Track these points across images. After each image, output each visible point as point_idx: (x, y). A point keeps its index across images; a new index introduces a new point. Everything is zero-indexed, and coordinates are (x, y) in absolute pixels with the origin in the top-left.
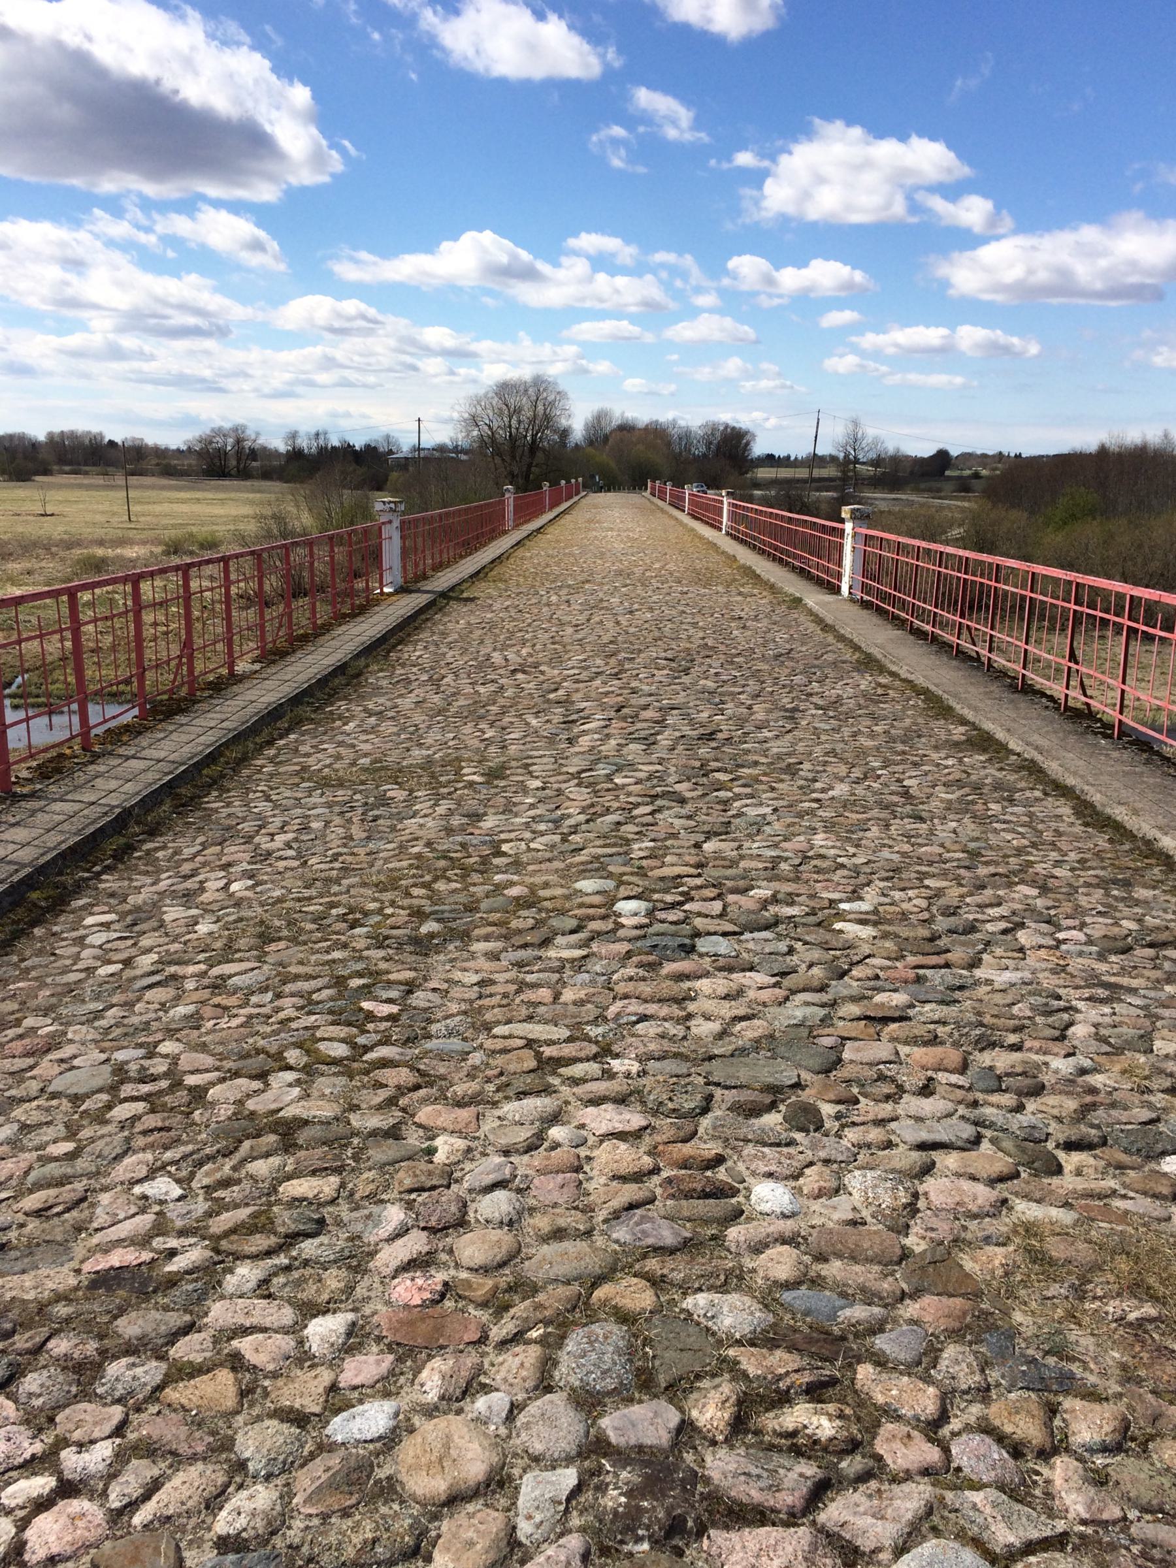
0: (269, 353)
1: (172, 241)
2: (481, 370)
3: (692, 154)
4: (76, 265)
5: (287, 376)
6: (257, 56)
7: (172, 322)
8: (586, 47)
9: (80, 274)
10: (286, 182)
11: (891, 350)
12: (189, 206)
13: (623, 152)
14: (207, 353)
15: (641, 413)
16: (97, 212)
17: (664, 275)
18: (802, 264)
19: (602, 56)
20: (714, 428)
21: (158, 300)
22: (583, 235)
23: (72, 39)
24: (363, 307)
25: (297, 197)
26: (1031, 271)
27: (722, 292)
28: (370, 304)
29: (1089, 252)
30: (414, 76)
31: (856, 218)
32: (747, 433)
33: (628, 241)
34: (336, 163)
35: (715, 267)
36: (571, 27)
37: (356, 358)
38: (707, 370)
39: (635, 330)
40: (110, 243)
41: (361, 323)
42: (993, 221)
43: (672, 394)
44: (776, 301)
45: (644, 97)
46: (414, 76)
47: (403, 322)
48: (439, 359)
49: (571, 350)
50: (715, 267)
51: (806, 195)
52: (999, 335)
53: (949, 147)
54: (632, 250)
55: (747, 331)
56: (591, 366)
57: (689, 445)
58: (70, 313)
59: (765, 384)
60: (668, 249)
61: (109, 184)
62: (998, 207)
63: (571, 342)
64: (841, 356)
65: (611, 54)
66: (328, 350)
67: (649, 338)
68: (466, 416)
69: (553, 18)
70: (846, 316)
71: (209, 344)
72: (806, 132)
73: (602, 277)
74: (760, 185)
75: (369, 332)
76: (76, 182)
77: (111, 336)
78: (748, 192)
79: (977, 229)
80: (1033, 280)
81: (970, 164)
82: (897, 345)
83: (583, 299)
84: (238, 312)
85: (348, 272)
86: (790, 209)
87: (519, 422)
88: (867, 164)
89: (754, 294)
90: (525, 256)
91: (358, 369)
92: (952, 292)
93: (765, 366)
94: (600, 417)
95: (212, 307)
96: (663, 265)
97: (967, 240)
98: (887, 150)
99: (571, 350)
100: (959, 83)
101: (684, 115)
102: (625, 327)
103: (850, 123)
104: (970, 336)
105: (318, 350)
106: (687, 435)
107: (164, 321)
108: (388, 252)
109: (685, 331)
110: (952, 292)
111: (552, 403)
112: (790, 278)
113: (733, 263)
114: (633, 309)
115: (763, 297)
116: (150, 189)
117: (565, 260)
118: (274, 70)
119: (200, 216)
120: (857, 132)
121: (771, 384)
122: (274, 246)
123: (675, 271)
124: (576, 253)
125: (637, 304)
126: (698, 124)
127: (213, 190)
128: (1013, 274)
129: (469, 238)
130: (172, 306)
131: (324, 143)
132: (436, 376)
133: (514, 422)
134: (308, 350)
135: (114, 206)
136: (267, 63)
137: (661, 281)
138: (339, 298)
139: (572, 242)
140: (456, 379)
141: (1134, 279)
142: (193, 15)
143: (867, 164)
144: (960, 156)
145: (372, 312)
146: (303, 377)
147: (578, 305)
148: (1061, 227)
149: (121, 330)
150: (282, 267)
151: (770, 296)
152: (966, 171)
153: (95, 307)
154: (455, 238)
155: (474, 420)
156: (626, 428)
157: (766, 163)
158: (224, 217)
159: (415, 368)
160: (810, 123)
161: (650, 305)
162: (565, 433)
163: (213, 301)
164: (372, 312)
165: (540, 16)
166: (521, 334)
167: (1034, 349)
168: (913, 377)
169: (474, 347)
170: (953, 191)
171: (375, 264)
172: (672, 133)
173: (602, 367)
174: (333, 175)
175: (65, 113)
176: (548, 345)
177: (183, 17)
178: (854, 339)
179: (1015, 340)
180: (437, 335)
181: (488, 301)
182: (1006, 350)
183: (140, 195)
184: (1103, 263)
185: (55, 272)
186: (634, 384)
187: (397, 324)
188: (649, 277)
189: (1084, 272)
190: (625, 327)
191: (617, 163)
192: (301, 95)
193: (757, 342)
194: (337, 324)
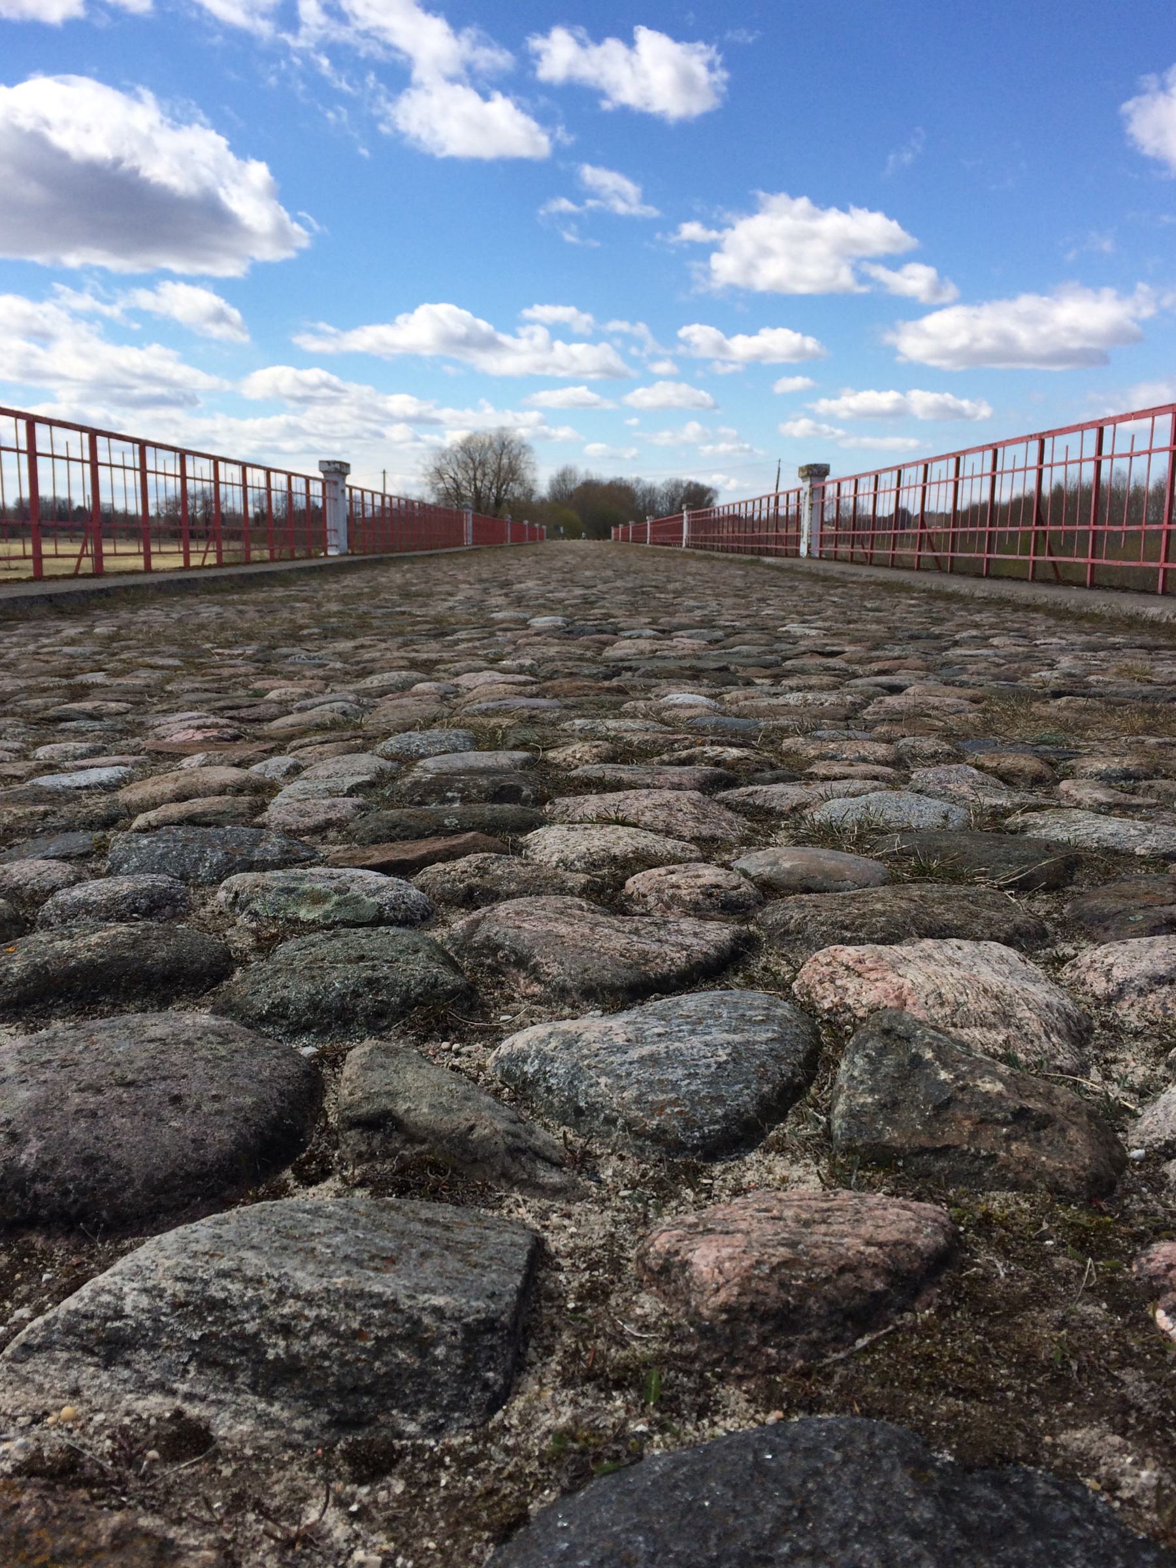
0: (233, 422)
1: (136, 314)
2: (443, 436)
3: (630, 224)
4: (44, 338)
5: (254, 444)
6: (212, 135)
7: (136, 392)
8: (534, 126)
9: (44, 346)
10: (252, 258)
11: (845, 414)
12: (149, 282)
13: (574, 227)
14: (172, 421)
15: (606, 473)
16: (59, 287)
17: (618, 342)
18: (752, 332)
19: (552, 137)
20: (677, 485)
21: (123, 370)
22: (537, 307)
23: (27, 123)
24: (324, 375)
25: (260, 270)
26: (975, 339)
27: (676, 360)
28: (331, 372)
29: (1031, 320)
30: (364, 152)
31: (803, 289)
32: (709, 490)
33: (582, 309)
34: (301, 237)
35: (667, 335)
36: (519, 106)
37: (321, 427)
38: (666, 434)
39: (593, 397)
40: (76, 315)
41: (325, 392)
42: (937, 289)
43: (634, 458)
44: (731, 368)
45: (592, 175)
46: (364, 152)
47: (367, 389)
48: (402, 426)
49: (534, 416)
50: (667, 335)
51: (750, 266)
52: (948, 398)
53: (890, 216)
54: (587, 318)
55: (703, 395)
56: (553, 432)
57: (653, 502)
58: (33, 383)
59: (723, 447)
60: (621, 318)
61: (72, 260)
62: (941, 274)
63: (531, 408)
64: (796, 420)
65: (560, 131)
66: (292, 419)
67: (609, 405)
68: (432, 469)
69: (498, 96)
70: (799, 382)
71: (175, 413)
72: (751, 208)
73: (559, 345)
74: (707, 259)
75: (330, 401)
76: (40, 259)
77: (75, 406)
78: (695, 264)
79: (924, 298)
80: (978, 346)
81: (913, 234)
82: (850, 410)
83: (544, 366)
84: (201, 380)
85: (310, 344)
86: (737, 280)
87: (484, 475)
88: (813, 235)
89: (708, 361)
90: (484, 325)
91: (323, 437)
92: (899, 359)
93: (723, 430)
94: (564, 477)
95: (177, 376)
96: (618, 334)
97: (914, 309)
98: (833, 222)
99: (534, 416)
100: (891, 158)
101: (630, 189)
102: (582, 392)
103: (794, 194)
104: (921, 400)
105: (282, 419)
106: (651, 491)
107: (130, 392)
108: (348, 324)
109: (643, 397)
110: (899, 359)
111: (517, 457)
112: (742, 346)
113: (683, 332)
114: (592, 376)
115: (718, 364)
116: (116, 264)
117: (523, 332)
118: (231, 148)
119: (161, 290)
120: (803, 203)
121: (730, 447)
122: (235, 314)
123: (628, 339)
124: (533, 322)
125: (596, 371)
126: (645, 199)
127: (177, 266)
128: (960, 341)
129: (424, 312)
130: (134, 375)
131: (286, 216)
132: (401, 442)
133: (479, 474)
134: (273, 420)
135: (74, 279)
136: (223, 142)
137: (615, 348)
138: (300, 367)
139: (528, 313)
140: (420, 445)
141: (1075, 345)
142: (148, 96)
143: (813, 235)
144: (903, 226)
145: (335, 380)
146: (269, 444)
147: (538, 373)
148: (1000, 297)
149: (86, 400)
150: (245, 339)
151: (724, 362)
152: (910, 242)
153: (61, 377)
154: (411, 309)
155: (439, 473)
156: (590, 487)
157: (714, 234)
158: (182, 290)
159: (380, 435)
160: (755, 197)
161: (608, 371)
162: (531, 492)
163: (181, 372)
164: (335, 380)
165: (486, 97)
166: (482, 401)
167: (985, 411)
168: (867, 441)
169: (435, 414)
170: (894, 262)
171: (336, 336)
172: (621, 208)
173: (564, 432)
174: (299, 250)
175: (33, 192)
176: (509, 412)
177: (138, 98)
178: (809, 406)
179: (965, 404)
180: (400, 403)
181: (449, 369)
182: (959, 413)
183: (103, 270)
184: (1044, 329)
185: (19, 345)
186: (595, 448)
187: (357, 390)
188: (604, 346)
189: (1025, 337)
190: (582, 392)
191: (569, 238)
192: (258, 172)
193: (716, 407)
194: (299, 393)
